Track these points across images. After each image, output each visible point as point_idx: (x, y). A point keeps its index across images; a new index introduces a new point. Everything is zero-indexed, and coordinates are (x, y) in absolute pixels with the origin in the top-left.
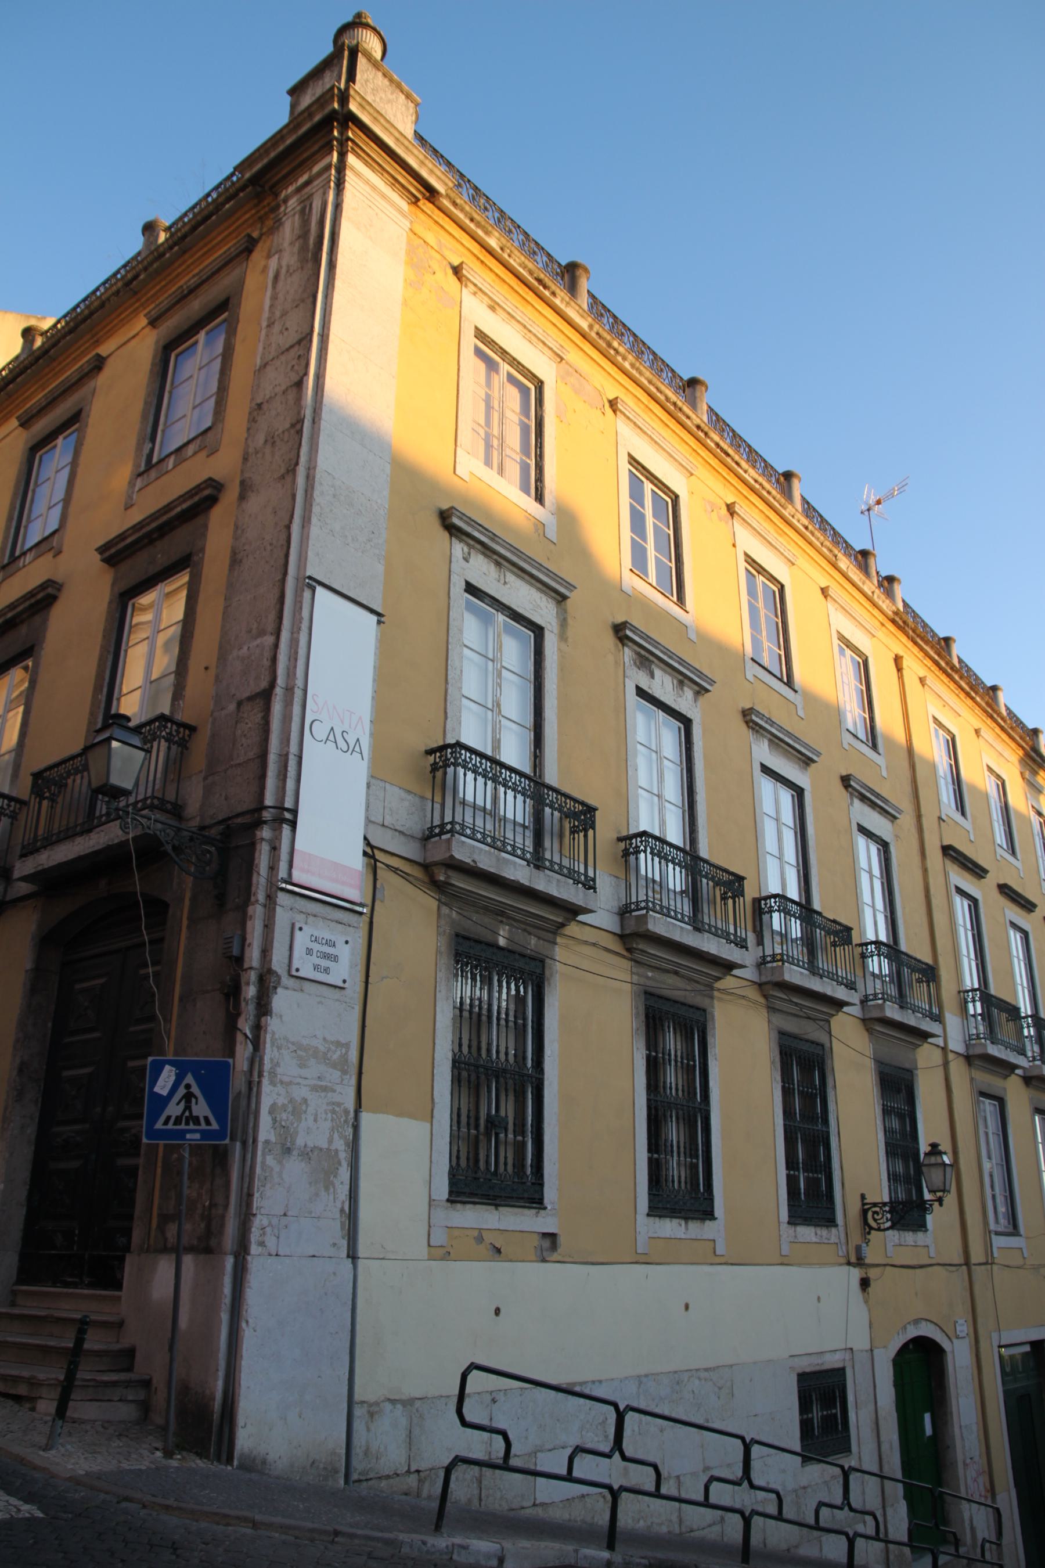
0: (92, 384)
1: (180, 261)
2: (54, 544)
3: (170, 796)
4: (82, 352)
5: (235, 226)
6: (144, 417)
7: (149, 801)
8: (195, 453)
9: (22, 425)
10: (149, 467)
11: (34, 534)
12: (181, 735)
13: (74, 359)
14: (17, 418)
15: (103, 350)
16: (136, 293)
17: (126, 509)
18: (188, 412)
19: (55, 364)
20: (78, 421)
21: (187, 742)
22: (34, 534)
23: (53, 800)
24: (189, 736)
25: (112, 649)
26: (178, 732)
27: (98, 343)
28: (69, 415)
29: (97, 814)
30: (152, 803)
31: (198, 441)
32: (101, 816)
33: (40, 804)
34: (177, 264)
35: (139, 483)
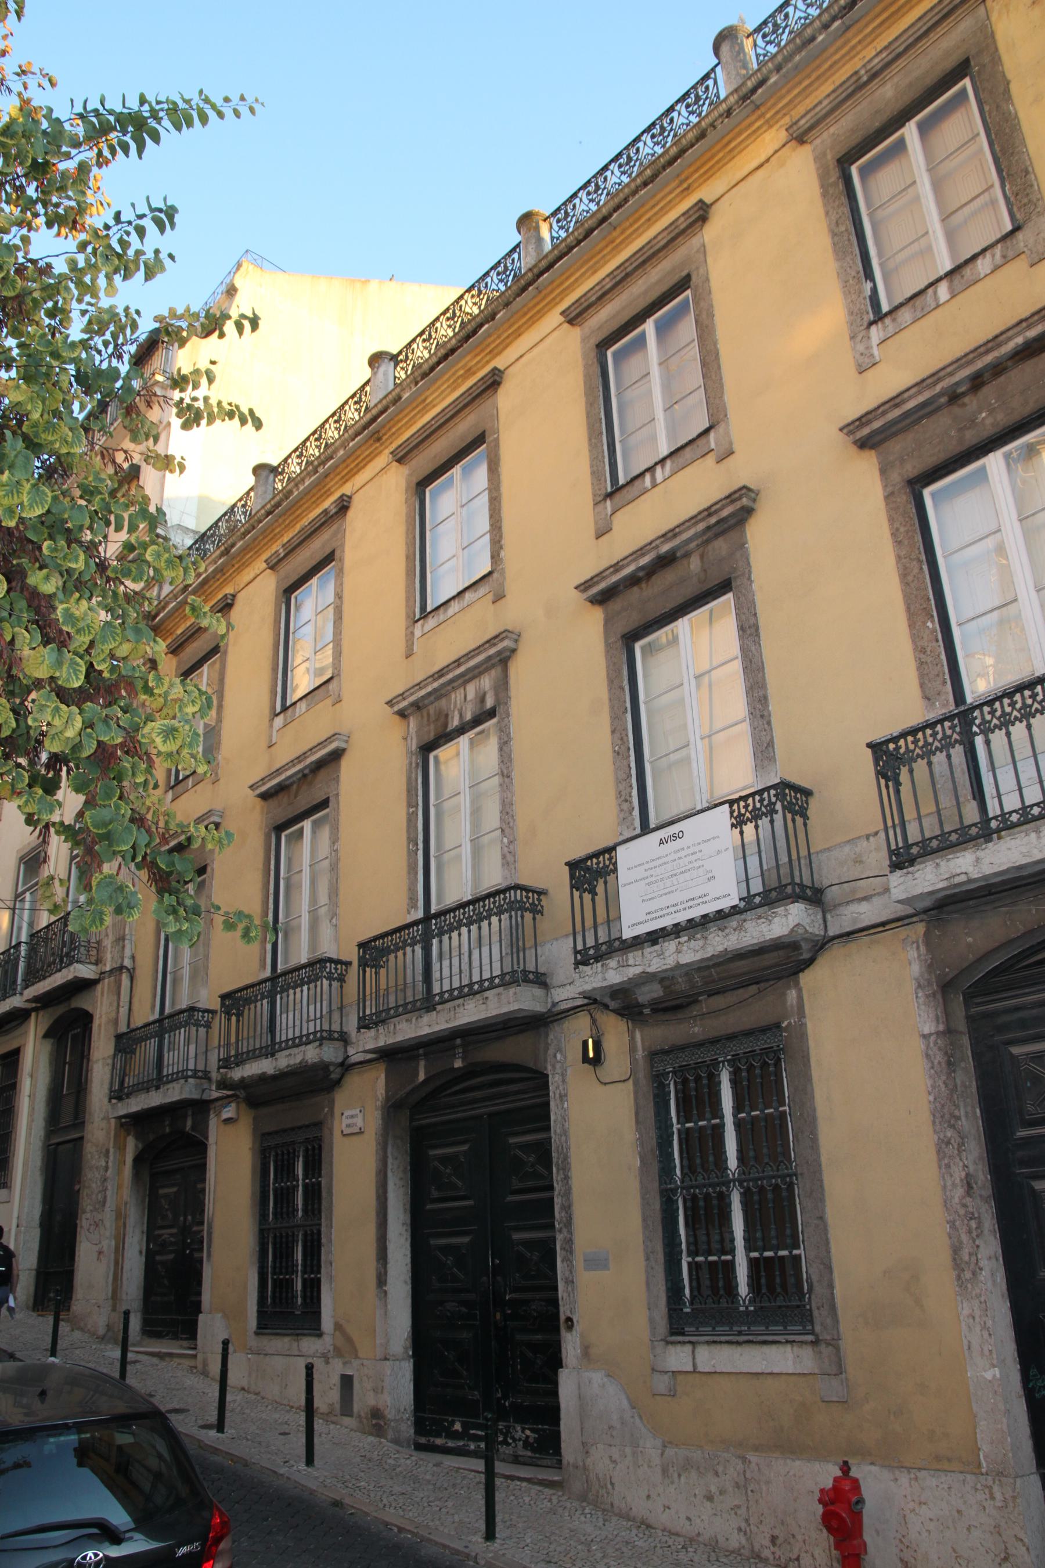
0: (695, 242)
1: (839, 43)
2: (713, 446)
3: (336, 1027)
4: (662, 209)
5: (702, 171)
6: (840, 252)
7: (319, 1035)
8: (996, 268)
9: (571, 322)
10: (615, 491)
11: (302, 682)
12: (531, 901)
13: (649, 220)
14: (562, 313)
15: (706, 193)
16: (758, 107)
17: (598, 537)
18: (457, 556)
19: (615, 234)
20: (333, 560)
21: (806, 809)
22: (302, 682)
23: (239, 1015)
24: (346, 971)
25: (923, 557)
26: (528, 898)
27: (495, 353)
28: (950, 64)
29: (165, 1073)
30: (321, 1036)
31: (998, 250)
32: (168, 1075)
33: (229, 1020)
34: (832, 50)
35: (279, 721)
